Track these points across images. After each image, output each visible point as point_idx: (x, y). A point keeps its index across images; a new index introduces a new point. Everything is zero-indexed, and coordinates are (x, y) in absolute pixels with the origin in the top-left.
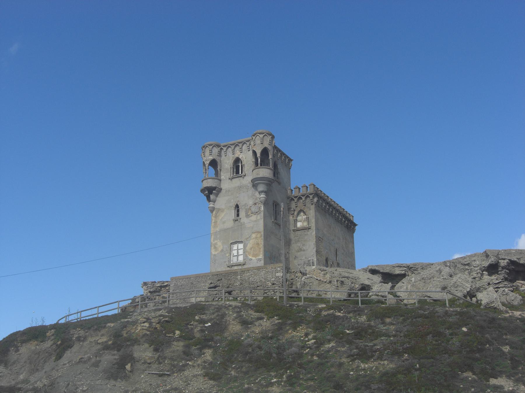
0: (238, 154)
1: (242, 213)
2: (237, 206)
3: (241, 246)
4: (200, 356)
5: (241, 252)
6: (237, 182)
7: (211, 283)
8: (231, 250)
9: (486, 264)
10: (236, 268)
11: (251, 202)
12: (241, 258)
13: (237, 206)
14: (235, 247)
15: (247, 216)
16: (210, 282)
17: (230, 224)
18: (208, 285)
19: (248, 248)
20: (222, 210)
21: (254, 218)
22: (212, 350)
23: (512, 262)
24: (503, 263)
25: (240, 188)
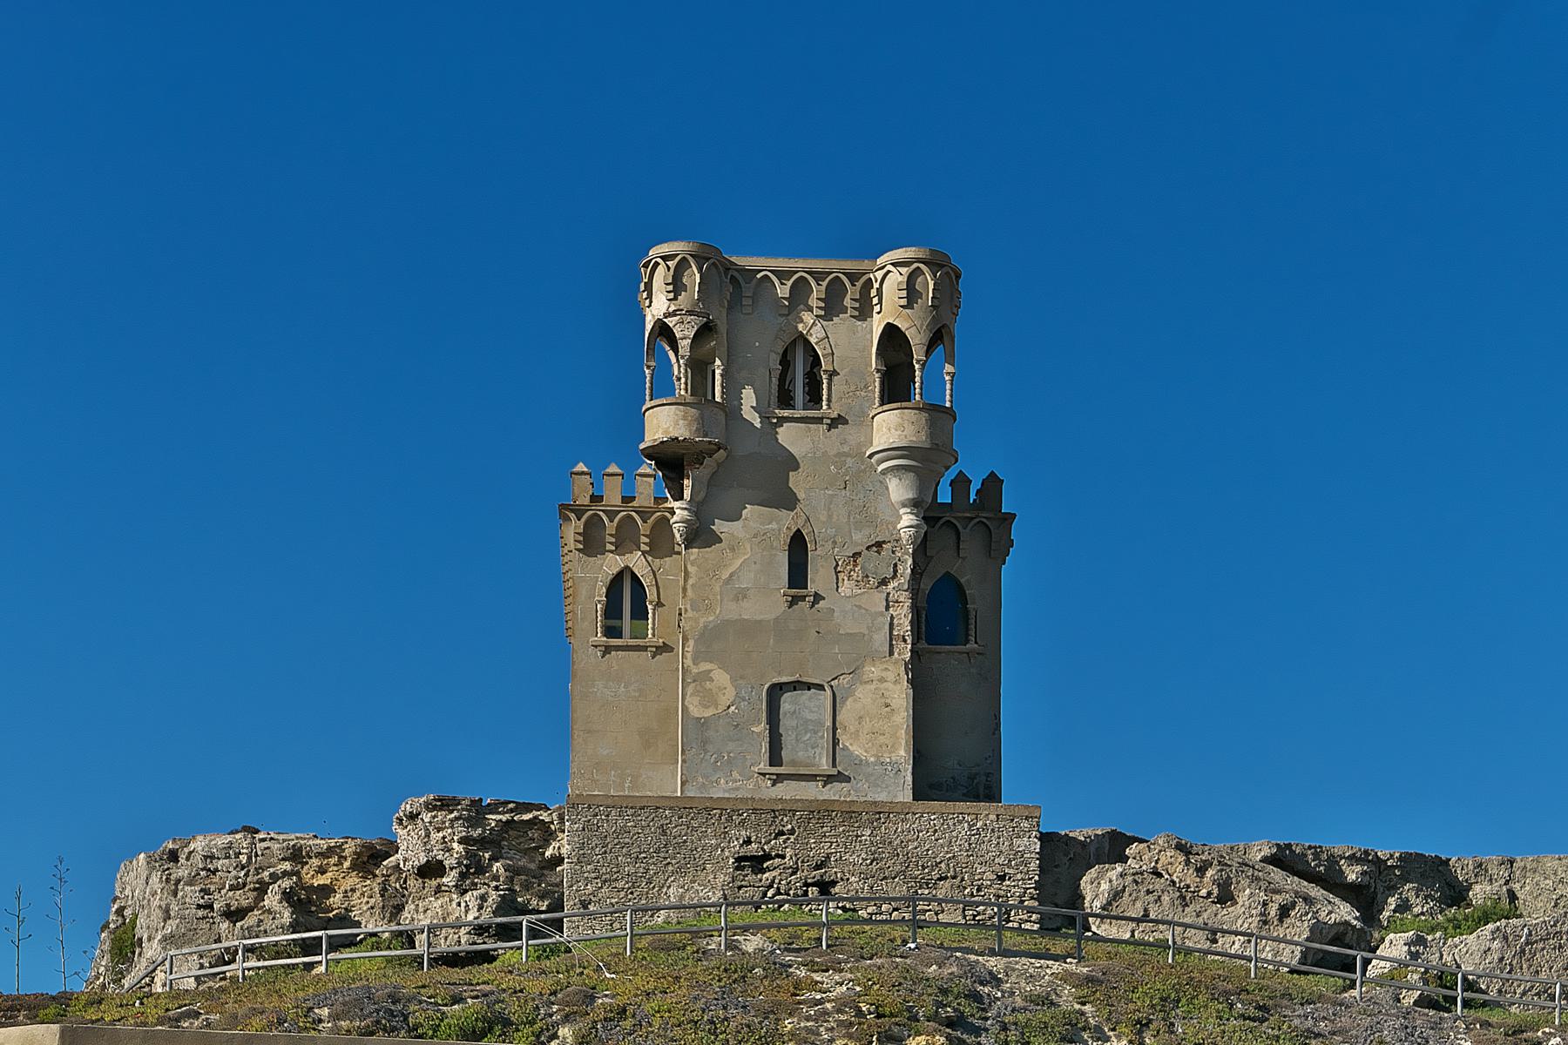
7: (748, 842)
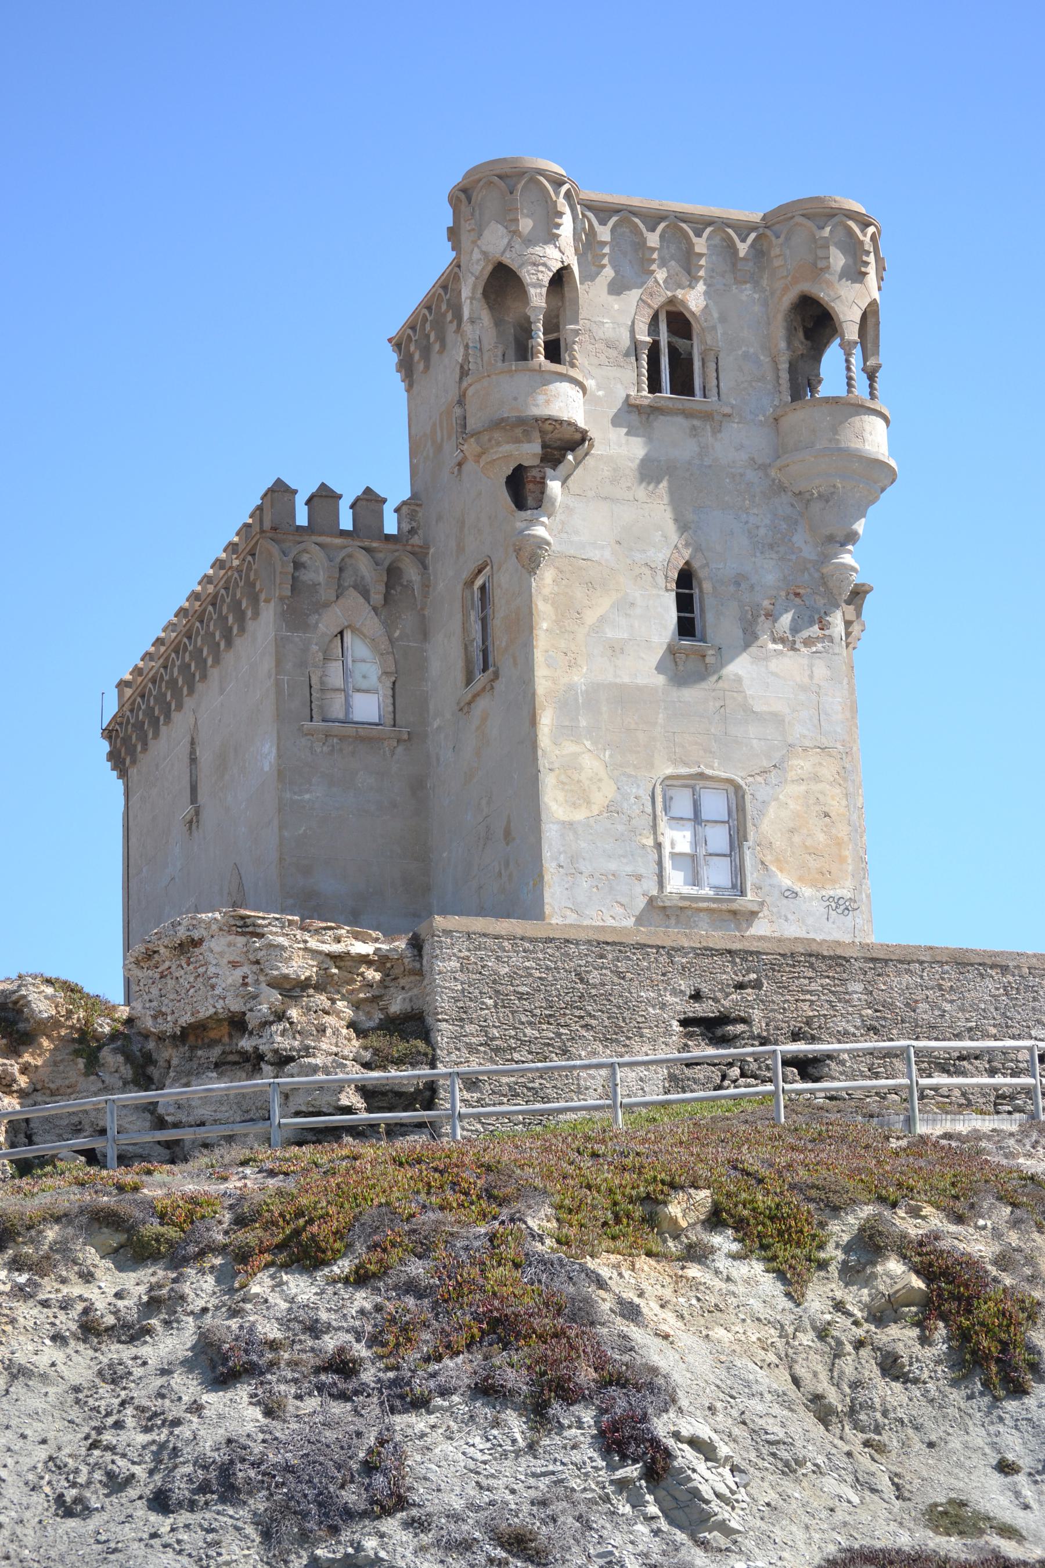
16: (685, 985)
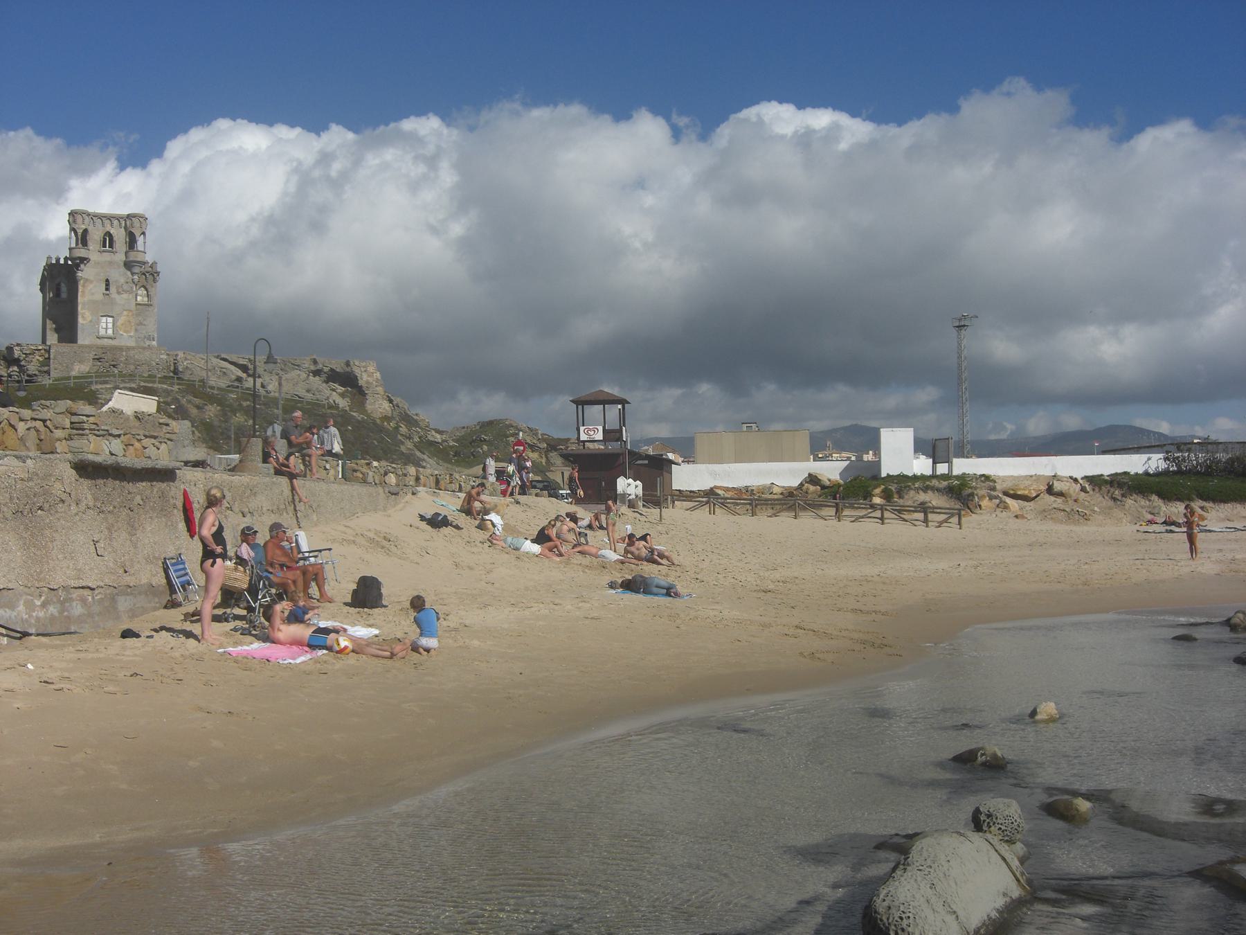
0: (108, 228)
1: (113, 289)
2: (107, 280)
3: (110, 320)
4: (170, 416)
5: (110, 325)
6: (107, 257)
8: (98, 322)
9: (313, 368)
10: (1117, 882)
11: (122, 280)
12: (110, 332)
13: (107, 280)
14: (104, 319)
15: (119, 293)
17: (99, 297)
18: (92, 356)
19: (119, 324)
20: (92, 282)
21: (125, 296)
22: (884, 475)
23: (332, 370)
24: (326, 369)
25: (111, 263)
